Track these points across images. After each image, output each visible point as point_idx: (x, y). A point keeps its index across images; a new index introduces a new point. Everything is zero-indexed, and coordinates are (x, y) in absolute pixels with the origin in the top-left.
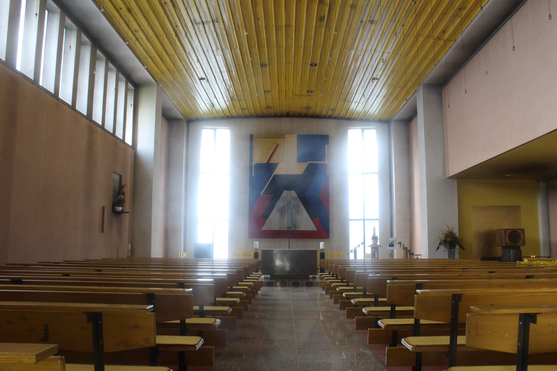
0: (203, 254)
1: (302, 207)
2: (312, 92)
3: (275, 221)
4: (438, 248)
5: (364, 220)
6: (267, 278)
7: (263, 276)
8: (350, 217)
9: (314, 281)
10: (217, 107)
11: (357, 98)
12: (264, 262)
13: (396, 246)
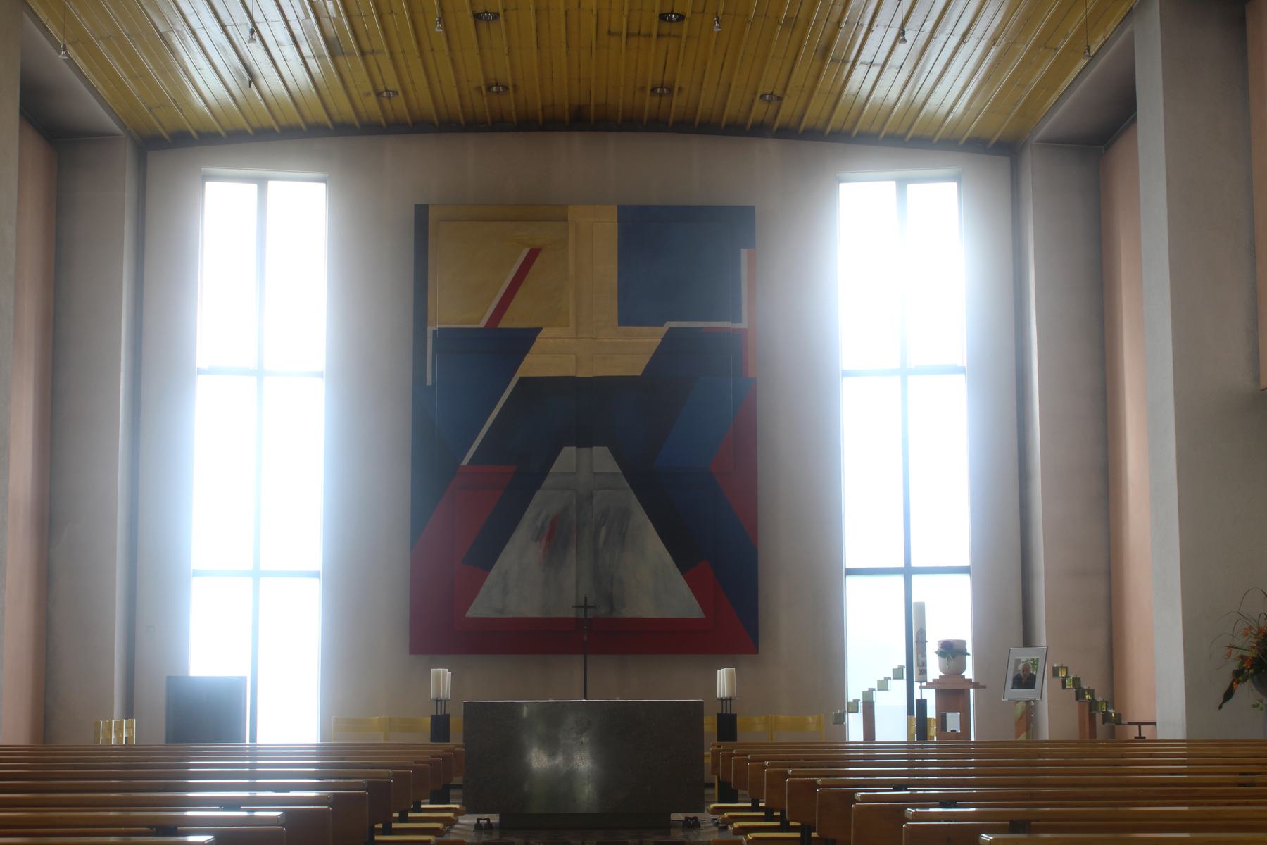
0: (205, 721)
1: (640, 516)
2: (681, 18)
3: (519, 583)
4: (1229, 694)
5: (259, 373)
6: (489, 826)
7: (468, 820)
8: (850, 561)
9: (692, 836)
10: (270, 81)
11: (878, 43)
12: (473, 759)
13: (1045, 683)
